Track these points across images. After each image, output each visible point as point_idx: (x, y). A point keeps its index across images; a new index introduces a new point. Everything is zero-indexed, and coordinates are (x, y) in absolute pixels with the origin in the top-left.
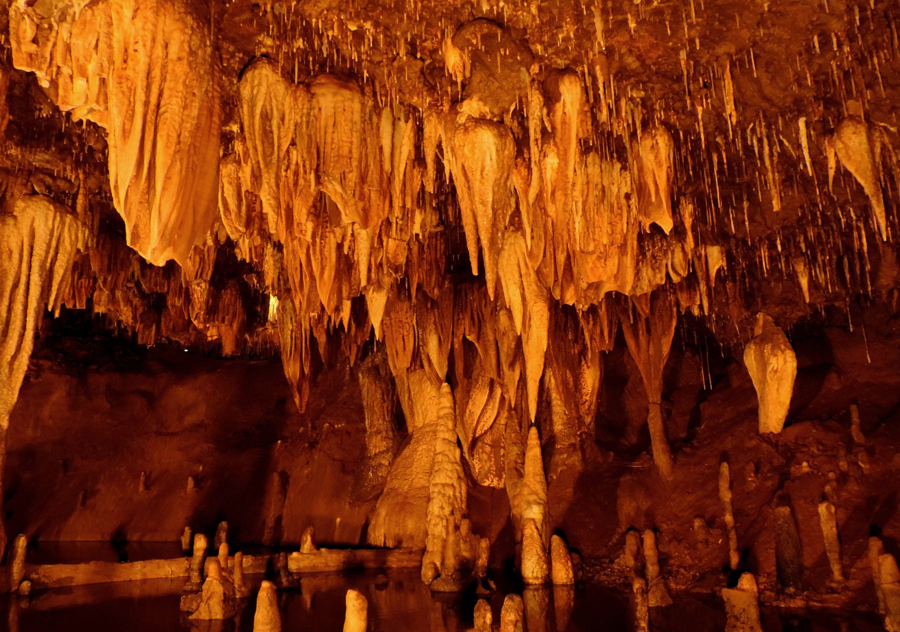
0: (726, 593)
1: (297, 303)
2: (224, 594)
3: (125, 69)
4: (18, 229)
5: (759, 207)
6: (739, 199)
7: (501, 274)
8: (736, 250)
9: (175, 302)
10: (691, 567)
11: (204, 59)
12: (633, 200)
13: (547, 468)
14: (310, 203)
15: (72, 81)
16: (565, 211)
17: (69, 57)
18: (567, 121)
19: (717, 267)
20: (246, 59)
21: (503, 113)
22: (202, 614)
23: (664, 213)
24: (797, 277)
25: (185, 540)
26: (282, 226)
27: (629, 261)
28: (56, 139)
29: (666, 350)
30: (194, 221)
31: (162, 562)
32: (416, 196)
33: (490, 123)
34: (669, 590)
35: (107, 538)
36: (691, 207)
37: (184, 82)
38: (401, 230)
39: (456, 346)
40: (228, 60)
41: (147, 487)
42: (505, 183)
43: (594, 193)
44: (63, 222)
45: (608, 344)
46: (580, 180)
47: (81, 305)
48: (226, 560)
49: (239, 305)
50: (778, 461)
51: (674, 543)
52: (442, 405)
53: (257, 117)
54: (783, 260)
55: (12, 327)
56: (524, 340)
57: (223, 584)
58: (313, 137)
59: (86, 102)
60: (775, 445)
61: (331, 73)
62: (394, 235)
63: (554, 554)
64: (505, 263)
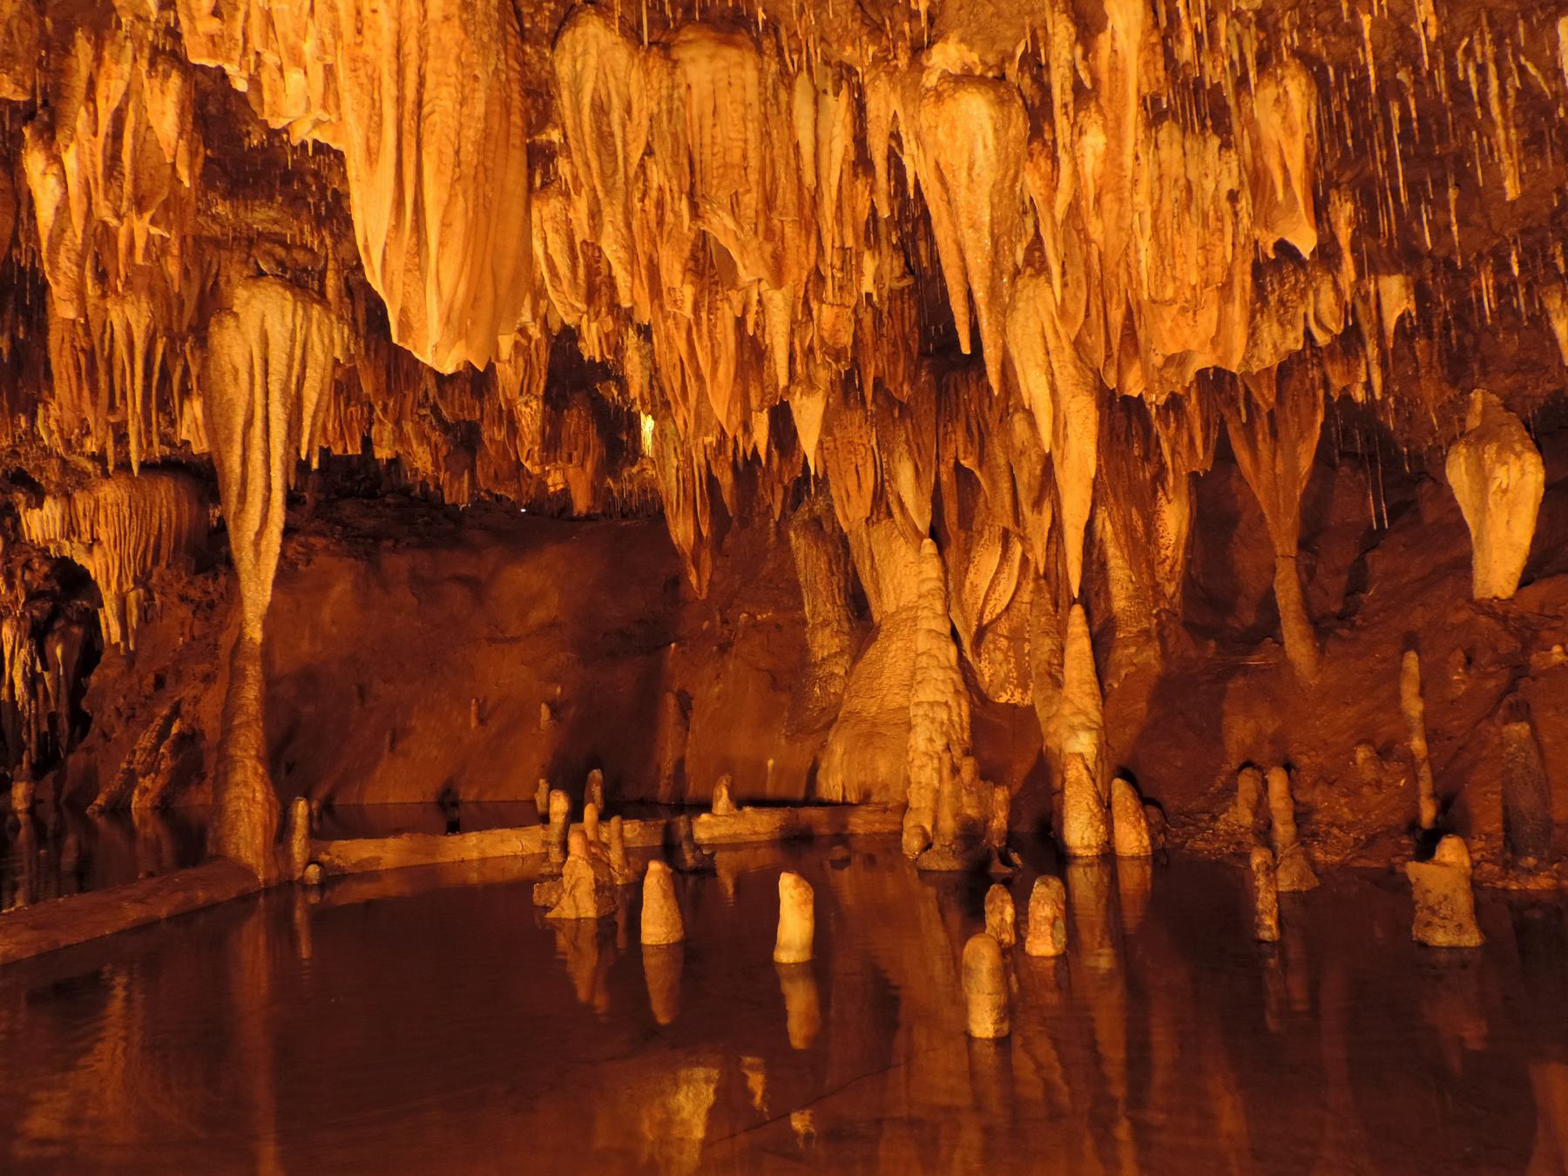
0: (1414, 869)
1: (680, 422)
2: (596, 881)
3: (361, 44)
4: (242, 334)
5: (1477, 198)
6: (1440, 185)
7: (1014, 352)
8: (1433, 279)
9: (494, 434)
10: (1351, 825)
11: (488, 15)
12: (1243, 202)
13: (1101, 673)
14: (687, 254)
15: (282, 76)
16: (1120, 229)
17: (272, 35)
18: (1120, 66)
19: (1398, 313)
20: (562, 11)
21: (1003, 61)
22: (566, 910)
23: (1300, 221)
24: (1549, 320)
25: (540, 798)
26: (643, 296)
27: (1237, 312)
28: (282, 183)
29: (1305, 463)
30: (496, 295)
31: (507, 832)
32: (862, 227)
33: (981, 80)
34: (1313, 864)
35: (432, 799)
36: (1349, 207)
37: (458, 58)
38: (841, 288)
39: (944, 478)
40: (532, 17)
41: (482, 721)
42: (1012, 187)
43: (1173, 194)
44: (308, 318)
45: (1202, 460)
46: (1147, 173)
47: (354, 449)
48: (597, 832)
49: (592, 431)
50: (1508, 645)
51: (1322, 787)
52: (923, 576)
53: (586, 110)
54: (1521, 291)
55: (250, 488)
56: (1056, 462)
57: (593, 866)
58: (681, 137)
59: (308, 110)
60: (1504, 619)
61: (703, 21)
62: (830, 298)
63: (1117, 809)
64: (1019, 332)
